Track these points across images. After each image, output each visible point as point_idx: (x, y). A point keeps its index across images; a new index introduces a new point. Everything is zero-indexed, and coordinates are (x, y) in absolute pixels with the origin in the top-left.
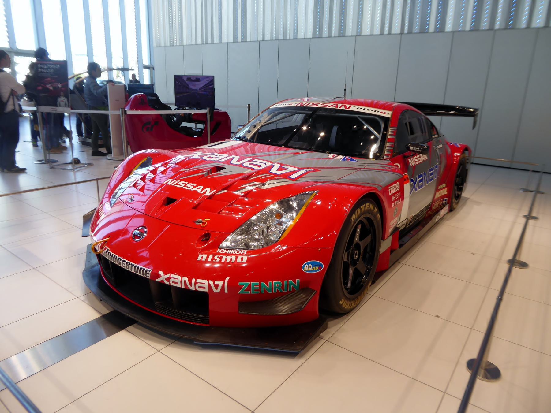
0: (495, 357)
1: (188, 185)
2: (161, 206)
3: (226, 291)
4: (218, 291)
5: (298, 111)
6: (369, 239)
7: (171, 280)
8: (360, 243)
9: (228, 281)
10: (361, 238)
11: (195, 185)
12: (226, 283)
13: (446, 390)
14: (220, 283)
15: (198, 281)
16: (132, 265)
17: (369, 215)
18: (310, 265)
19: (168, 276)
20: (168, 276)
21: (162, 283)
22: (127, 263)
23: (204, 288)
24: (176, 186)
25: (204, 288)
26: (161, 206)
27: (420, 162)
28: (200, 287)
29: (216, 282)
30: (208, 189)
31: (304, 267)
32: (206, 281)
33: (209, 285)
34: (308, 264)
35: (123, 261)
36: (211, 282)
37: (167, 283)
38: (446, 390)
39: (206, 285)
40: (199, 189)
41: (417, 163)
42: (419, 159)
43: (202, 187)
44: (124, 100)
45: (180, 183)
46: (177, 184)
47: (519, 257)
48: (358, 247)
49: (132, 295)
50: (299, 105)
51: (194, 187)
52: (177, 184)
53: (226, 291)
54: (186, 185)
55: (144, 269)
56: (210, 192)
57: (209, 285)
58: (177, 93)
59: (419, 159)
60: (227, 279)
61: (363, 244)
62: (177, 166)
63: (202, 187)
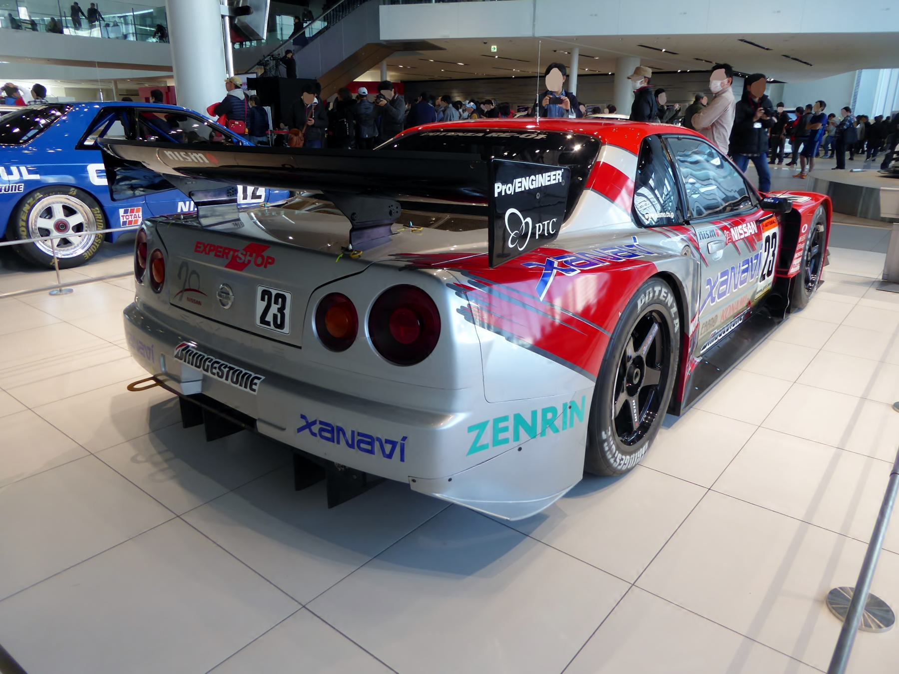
8: (629, 398)
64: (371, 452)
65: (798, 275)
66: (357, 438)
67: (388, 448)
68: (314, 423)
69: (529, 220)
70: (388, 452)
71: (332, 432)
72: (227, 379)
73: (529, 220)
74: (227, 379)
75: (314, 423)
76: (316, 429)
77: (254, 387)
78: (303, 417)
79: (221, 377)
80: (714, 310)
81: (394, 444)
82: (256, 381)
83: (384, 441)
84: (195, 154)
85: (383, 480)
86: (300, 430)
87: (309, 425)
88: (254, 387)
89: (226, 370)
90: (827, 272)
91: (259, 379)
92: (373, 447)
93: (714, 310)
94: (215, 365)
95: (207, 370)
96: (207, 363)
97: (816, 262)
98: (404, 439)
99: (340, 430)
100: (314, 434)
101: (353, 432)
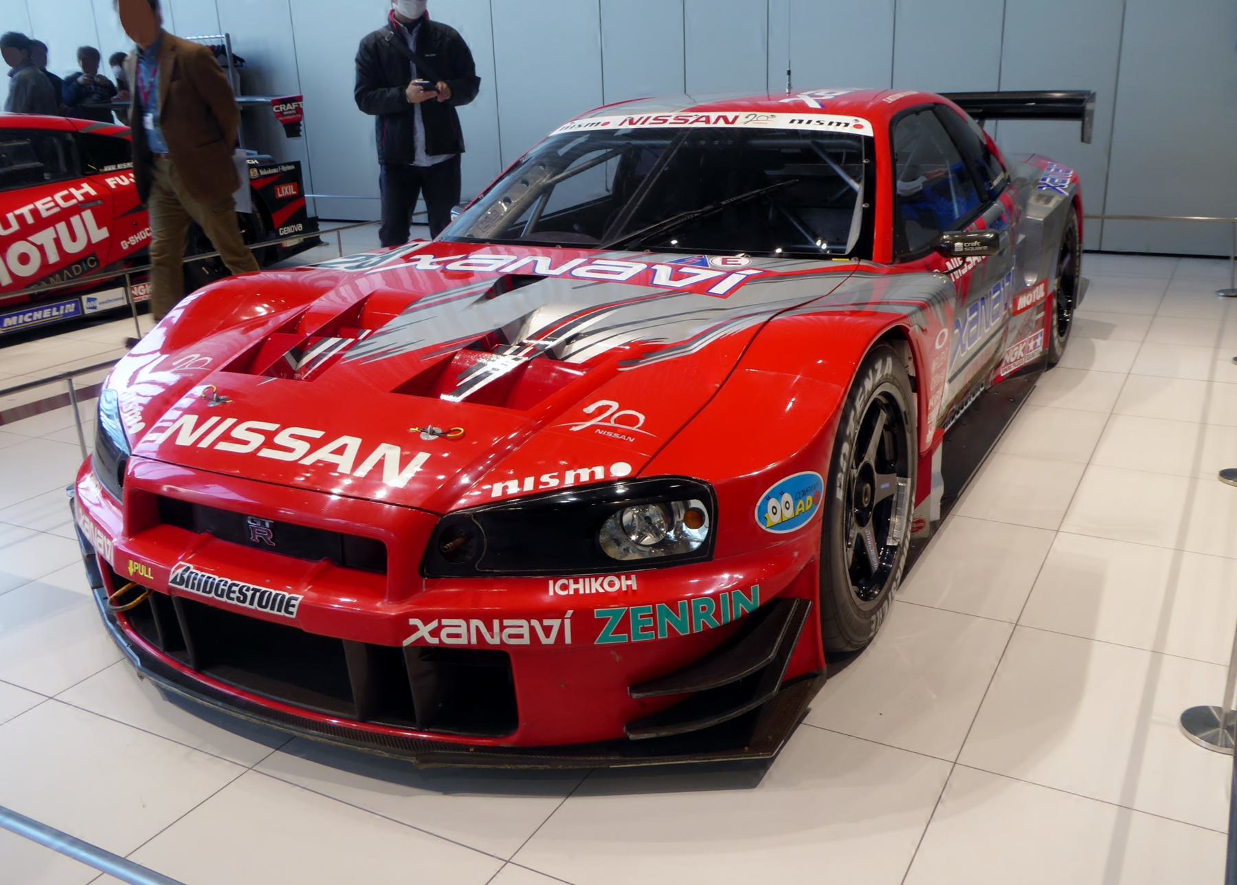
1: (282, 439)
2: (327, 244)
3: (568, 640)
4: (551, 640)
7: (444, 633)
9: (572, 618)
11: (317, 434)
12: (568, 623)
13: (1109, 218)
14: (556, 623)
15: (506, 622)
18: (787, 497)
19: (434, 624)
20: (434, 624)
21: (421, 647)
23: (521, 636)
24: (222, 446)
25: (521, 636)
26: (327, 244)
28: (510, 636)
29: (547, 622)
30: (389, 452)
31: (763, 511)
32: (523, 622)
33: (532, 629)
34: (779, 494)
36: (535, 623)
37: (435, 641)
38: (1109, 218)
39: (525, 631)
40: (340, 451)
43: (353, 443)
45: (239, 433)
46: (226, 437)
50: (626, 126)
51: (315, 445)
52: (226, 437)
53: (568, 640)
54: (269, 443)
56: (404, 462)
57: (532, 629)
60: (570, 613)
62: (158, 74)
63: (353, 443)
74: (251, 603)
77: (291, 609)
94: (234, 588)
96: (221, 587)
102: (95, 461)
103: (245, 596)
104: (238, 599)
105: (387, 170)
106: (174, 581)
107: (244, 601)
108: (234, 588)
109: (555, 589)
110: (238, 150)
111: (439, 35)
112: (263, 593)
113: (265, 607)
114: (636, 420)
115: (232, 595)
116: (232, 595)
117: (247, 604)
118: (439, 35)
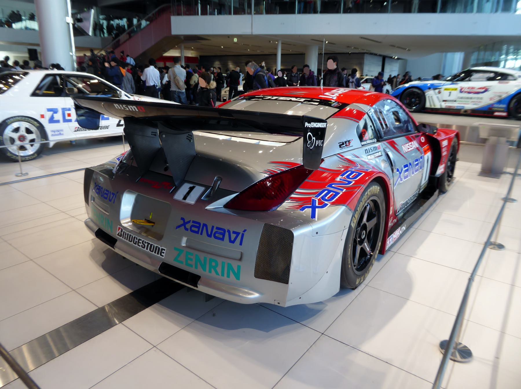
0: (465, 339)
5: (379, 244)
6: (374, 221)
8: (367, 224)
10: (368, 220)
16: (149, 244)
17: (371, 198)
22: (143, 241)
27: (412, 149)
35: (139, 240)
41: (410, 150)
42: (411, 146)
44: (55, 63)
47: (458, 339)
48: (365, 227)
49: (195, 279)
55: (130, 235)
58: (261, 181)
59: (411, 146)
61: (370, 225)
64: (222, 239)
65: (443, 175)
66: (215, 230)
67: (233, 236)
68: (189, 222)
69: (314, 138)
70: (232, 239)
71: (198, 228)
72: (147, 249)
73: (314, 138)
74: (147, 249)
75: (189, 222)
76: (188, 226)
77: (162, 254)
78: (182, 219)
79: (144, 248)
80: (404, 189)
81: (237, 234)
82: (163, 251)
83: (231, 232)
84: (131, 106)
85: (226, 300)
86: (179, 227)
87: (185, 224)
88: (162, 254)
89: (146, 245)
90: (457, 173)
91: (164, 250)
92: (224, 236)
93: (404, 189)
94: (140, 241)
95: (135, 244)
96: (135, 240)
97: (451, 168)
98: (245, 231)
99: (205, 225)
100: (186, 229)
101: (213, 227)
102: (362, 168)
103: (145, 245)
104: (142, 246)
105: (172, 49)
106: (118, 235)
107: (144, 248)
108: (140, 241)
109: (182, 25)
110: (152, 67)
111: (182, 9)
112: (151, 245)
113: (152, 251)
114: (310, 135)
115: (140, 244)
116: (140, 244)
117: (145, 249)
118: (182, 9)
